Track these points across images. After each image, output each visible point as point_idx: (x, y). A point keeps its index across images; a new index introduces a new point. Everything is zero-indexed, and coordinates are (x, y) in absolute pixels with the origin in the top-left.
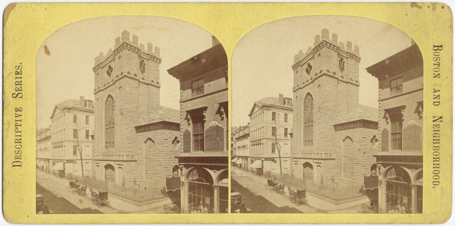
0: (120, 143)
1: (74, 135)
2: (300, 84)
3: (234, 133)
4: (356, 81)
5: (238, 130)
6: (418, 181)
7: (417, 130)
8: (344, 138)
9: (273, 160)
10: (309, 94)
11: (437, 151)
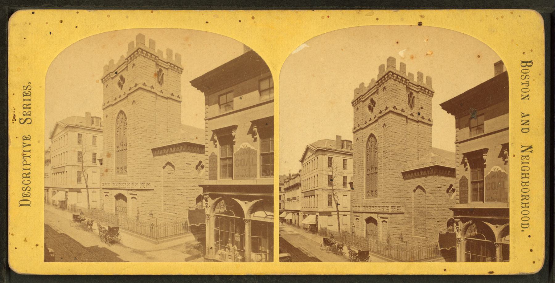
1: (78, 159)
2: (361, 124)
3: (283, 182)
4: (428, 120)
5: (287, 179)
6: (253, 214)
7: (502, 177)
8: (414, 188)
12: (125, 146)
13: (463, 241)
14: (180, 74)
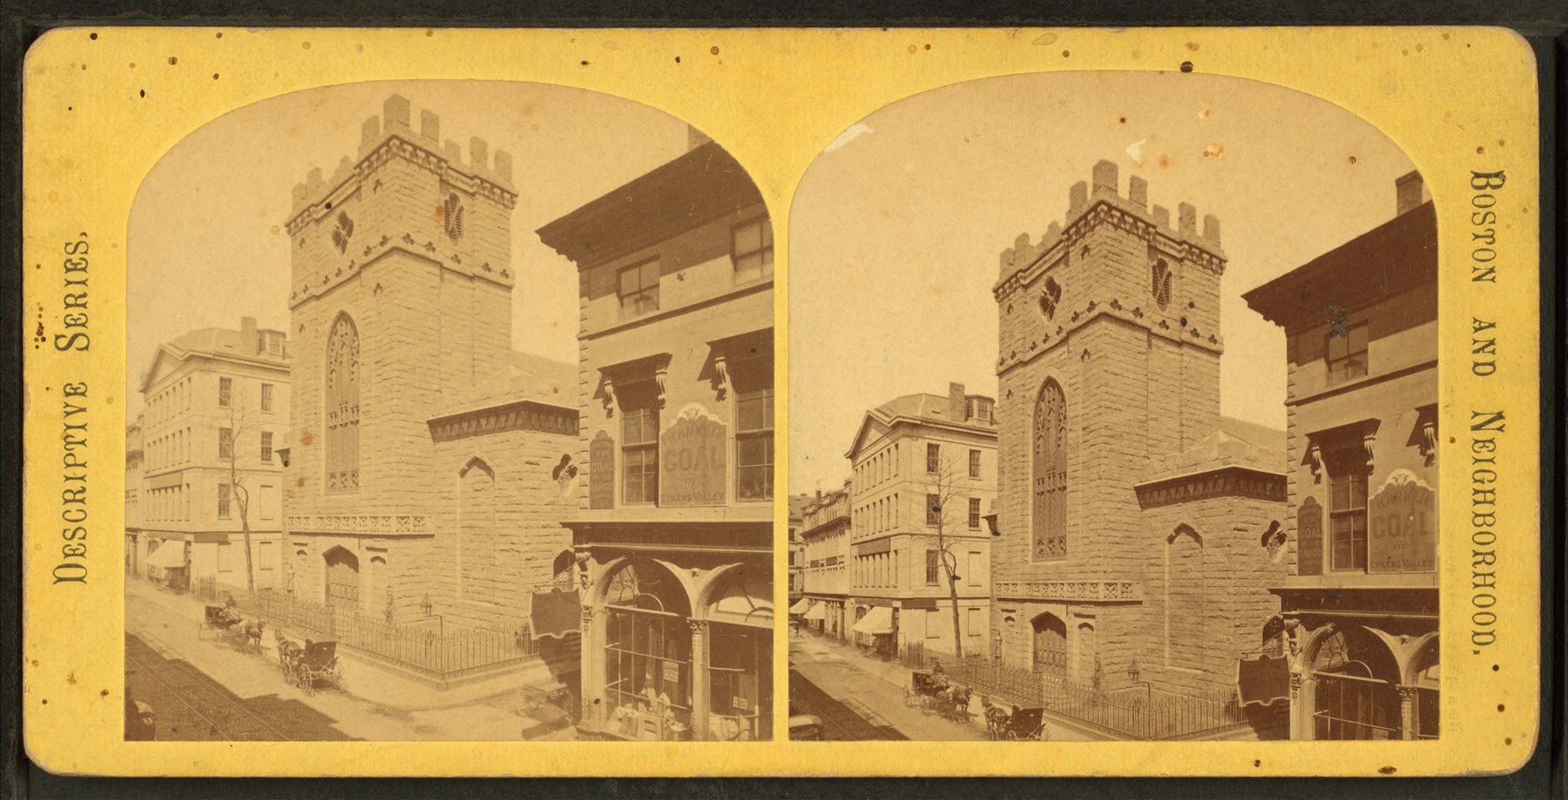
1: (220, 448)
2: (1020, 349)
3: (799, 515)
4: (501, 273)
6: (1422, 673)
7: (1420, 501)
8: (1171, 532)
11: (1485, 529)
12: (353, 412)
13: (1308, 682)
14: (509, 210)
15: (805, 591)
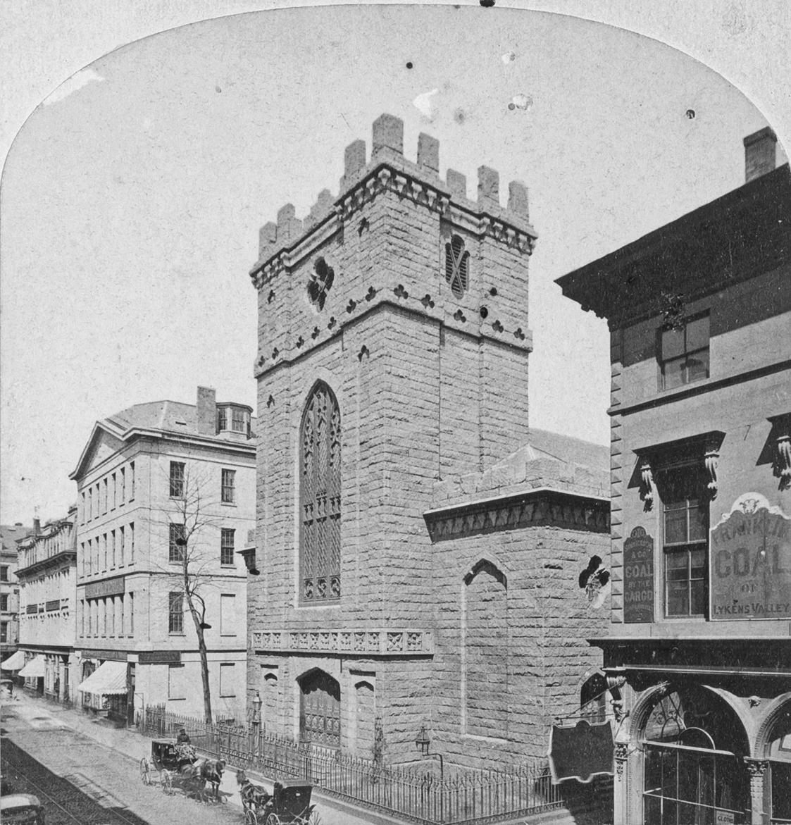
0: (364, 581)
2: (284, 346)
4: (515, 333)
6: (776, 743)
8: (468, 569)
9: (173, 659)
10: (321, 387)
13: (637, 753)
15: (20, 643)
